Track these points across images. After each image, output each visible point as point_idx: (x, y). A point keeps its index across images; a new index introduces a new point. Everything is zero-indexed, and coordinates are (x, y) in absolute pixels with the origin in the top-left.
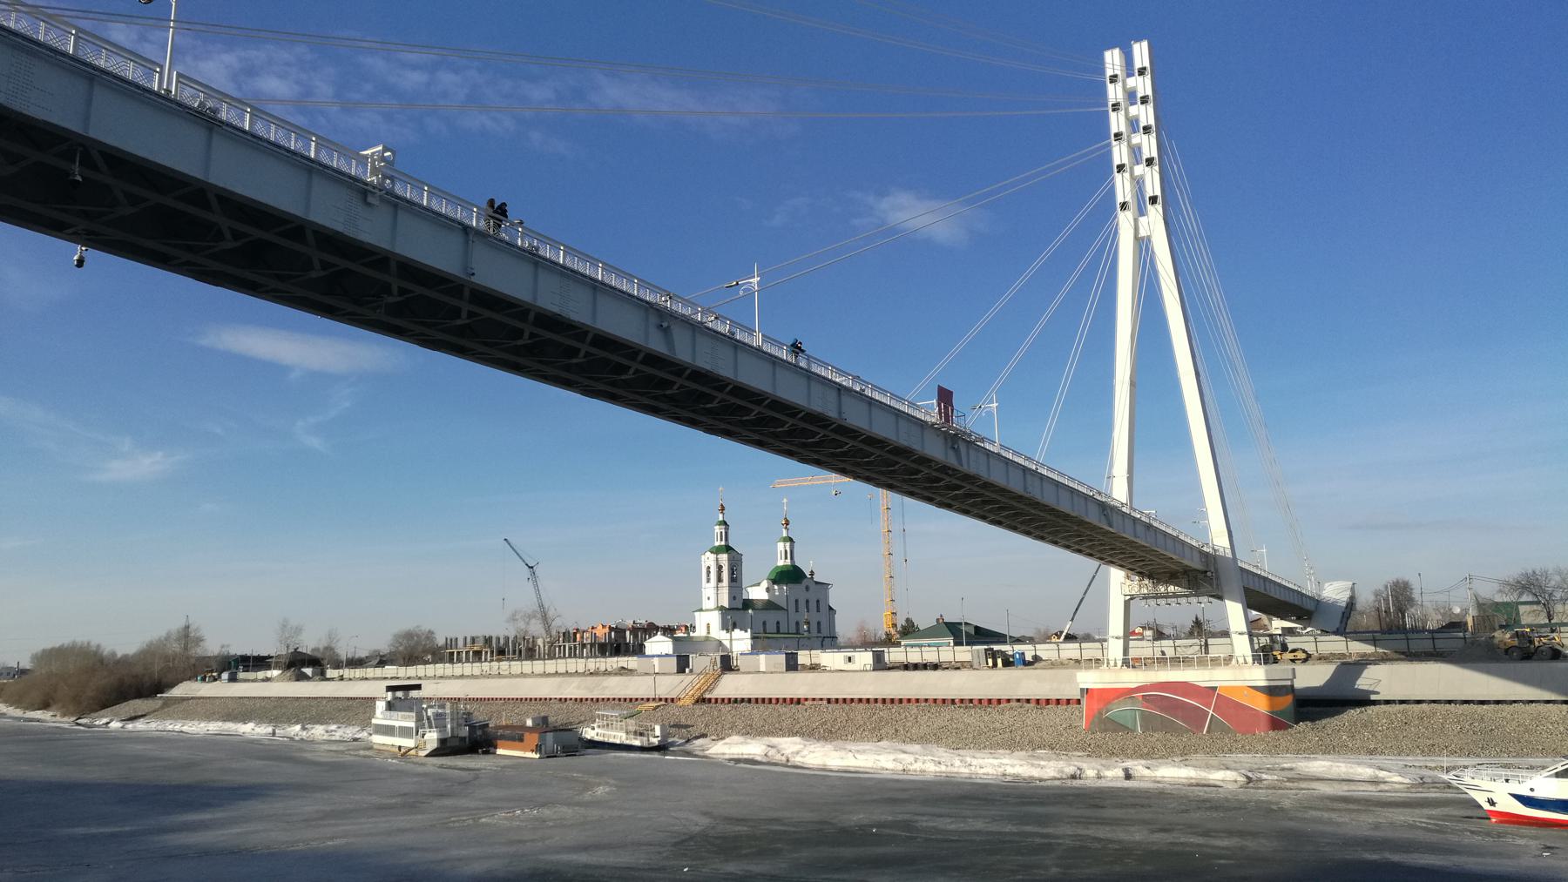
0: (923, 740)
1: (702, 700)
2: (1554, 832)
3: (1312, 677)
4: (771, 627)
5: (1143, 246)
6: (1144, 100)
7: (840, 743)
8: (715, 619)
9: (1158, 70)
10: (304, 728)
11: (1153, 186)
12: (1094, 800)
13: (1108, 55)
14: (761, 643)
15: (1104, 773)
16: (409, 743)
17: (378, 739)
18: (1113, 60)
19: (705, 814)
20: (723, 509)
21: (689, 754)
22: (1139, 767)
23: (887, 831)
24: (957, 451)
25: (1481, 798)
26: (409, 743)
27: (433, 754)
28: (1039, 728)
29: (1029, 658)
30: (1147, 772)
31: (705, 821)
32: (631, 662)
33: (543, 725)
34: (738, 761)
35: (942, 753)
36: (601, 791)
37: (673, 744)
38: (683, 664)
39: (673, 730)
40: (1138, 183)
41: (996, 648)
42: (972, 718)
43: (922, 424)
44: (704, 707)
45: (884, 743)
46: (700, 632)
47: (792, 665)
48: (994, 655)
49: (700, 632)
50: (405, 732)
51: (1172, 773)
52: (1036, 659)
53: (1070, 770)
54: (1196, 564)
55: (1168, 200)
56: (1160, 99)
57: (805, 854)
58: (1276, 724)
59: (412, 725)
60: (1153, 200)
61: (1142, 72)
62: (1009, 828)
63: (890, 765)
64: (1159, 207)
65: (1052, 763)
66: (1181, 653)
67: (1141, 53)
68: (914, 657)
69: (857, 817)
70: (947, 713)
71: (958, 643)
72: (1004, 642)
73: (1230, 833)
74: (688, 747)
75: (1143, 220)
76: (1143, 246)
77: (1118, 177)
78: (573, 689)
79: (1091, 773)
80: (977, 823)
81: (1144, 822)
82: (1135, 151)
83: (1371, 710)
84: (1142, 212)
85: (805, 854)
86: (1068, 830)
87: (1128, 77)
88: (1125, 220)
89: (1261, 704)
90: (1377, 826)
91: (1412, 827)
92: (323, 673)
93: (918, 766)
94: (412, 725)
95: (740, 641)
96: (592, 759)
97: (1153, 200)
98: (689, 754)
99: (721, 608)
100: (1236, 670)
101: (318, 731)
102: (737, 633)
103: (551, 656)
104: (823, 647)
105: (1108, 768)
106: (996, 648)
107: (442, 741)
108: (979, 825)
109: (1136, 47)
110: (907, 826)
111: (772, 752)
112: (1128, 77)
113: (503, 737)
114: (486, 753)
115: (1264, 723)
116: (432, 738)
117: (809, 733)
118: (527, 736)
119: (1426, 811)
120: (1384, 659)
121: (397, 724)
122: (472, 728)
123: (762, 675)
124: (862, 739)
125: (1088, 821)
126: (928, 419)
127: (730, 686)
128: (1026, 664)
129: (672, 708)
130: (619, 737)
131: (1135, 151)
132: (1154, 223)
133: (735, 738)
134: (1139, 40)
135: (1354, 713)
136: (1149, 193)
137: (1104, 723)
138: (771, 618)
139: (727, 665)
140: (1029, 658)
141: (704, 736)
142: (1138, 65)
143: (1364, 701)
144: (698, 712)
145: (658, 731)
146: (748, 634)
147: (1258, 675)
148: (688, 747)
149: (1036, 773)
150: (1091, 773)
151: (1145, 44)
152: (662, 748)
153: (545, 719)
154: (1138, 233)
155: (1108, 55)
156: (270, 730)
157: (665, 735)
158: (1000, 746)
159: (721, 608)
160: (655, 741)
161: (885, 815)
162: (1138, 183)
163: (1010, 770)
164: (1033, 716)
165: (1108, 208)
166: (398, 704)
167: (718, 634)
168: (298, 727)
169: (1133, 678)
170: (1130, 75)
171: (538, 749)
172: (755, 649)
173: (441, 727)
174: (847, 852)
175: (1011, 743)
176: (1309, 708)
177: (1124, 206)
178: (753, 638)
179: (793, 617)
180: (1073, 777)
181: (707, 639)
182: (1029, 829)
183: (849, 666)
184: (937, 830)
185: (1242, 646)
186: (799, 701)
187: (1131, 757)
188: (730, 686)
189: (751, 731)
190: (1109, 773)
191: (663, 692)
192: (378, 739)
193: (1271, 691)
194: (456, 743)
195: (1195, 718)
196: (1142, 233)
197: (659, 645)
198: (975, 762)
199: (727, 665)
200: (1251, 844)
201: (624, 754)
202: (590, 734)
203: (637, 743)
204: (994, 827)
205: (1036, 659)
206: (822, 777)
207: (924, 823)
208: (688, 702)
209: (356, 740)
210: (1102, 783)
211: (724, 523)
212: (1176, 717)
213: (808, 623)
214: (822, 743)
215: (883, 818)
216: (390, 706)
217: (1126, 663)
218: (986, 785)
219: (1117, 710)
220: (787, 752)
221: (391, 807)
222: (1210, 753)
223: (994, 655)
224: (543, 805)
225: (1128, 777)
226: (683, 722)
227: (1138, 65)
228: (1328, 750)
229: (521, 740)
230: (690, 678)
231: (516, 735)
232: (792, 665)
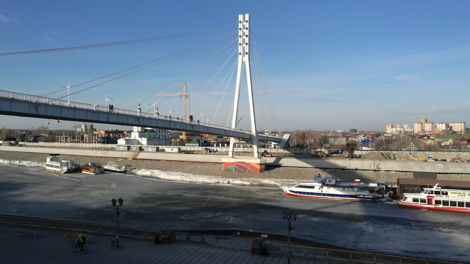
0: (187, 172)
1: (134, 159)
2: (292, 197)
3: (270, 160)
4: (152, 137)
5: (243, 63)
6: (247, 28)
7: (168, 172)
8: (137, 134)
9: (250, 22)
10: (20, 162)
11: (247, 50)
12: (217, 189)
13: (240, 15)
14: (150, 142)
15: (223, 182)
16: (59, 170)
17: (48, 168)
18: (241, 17)
19: (139, 192)
20: (140, 105)
21: (132, 173)
22: (231, 181)
23: (176, 197)
24: (193, 128)
25: (284, 190)
26: (59, 170)
27: (65, 173)
28: (213, 170)
29: (215, 150)
30: (232, 182)
31: (139, 194)
32: (114, 146)
33: (94, 165)
34: (144, 176)
35: (191, 176)
36: (114, 185)
37: (127, 171)
38: (129, 148)
39: (127, 167)
40: (244, 48)
41: (208, 148)
42: (199, 166)
43: (186, 124)
44: (135, 160)
45: (179, 173)
46: (133, 137)
47: (158, 150)
48: (207, 149)
49: (133, 137)
50: (57, 167)
51: (238, 182)
52: (217, 151)
53: (217, 181)
54: (248, 137)
55: (249, 53)
56: (250, 29)
57: (160, 202)
58: (261, 171)
59: (59, 165)
60: (247, 53)
61: (247, 21)
62: (200, 196)
63: (179, 179)
64: (248, 55)
65: (214, 179)
66: (249, 151)
67: (247, 16)
68: (188, 149)
69: (171, 193)
70: (194, 165)
71: (199, 146)
72: (210, 146)
73: (239, 197)
74: (131, 171)
75: (244, 57)
76: (243, 63)
77: (239, 56)
78: (99, 154)
79: (221, 182)
80: (194, 195)
81: (225, 195)
82: (244, 40)
83: (281, 168)
84: (244, 56)
85: (160, 202)
86: (210, 197)
87: (243, 20)
88: (240, 57)
89: (258, 167)
90: (265, 196)
91: (271, 196)
92: (17, 143)
93: (185, 179)
94: (59, 165)
95: (144, 141)
96: (108, 175)
97: (247, 53)
98: (132, 173)
99: (139, 132)
100: (255, 161)
101: (25, 163)
102: (143, 138)
103: (89, 142)
104: (166, 145)
105: (225, 180)
106: (208, 148)
107: (68, 170)
108: (194, 195)
109: (246, 15)
110: (180, 195)
111: (152, 174)
112: (243, 20)
113: (83, 168)
114: (80, 172)
115: (259, 171)
116: (65, 169)
117: (161, 169)
118: (91, 169)
119: (275, 192)
120: (290, 156)
121: (54, 165)
122: (76, 166)
123: (150, 153)
124: (174, 171)
125: (214, 195)
126: (186, 122)
127: (142, 155)
128: (214, 152)
129: (126, 161)
130: (114, 169)
131: (244, 40)
132: (246, 58)
133: (143, 170)
134: (247, 13)
135: (277, 169)
136: (246, 52)
137: (228, 170)
138: (152, 134)
139: (141, 149)
140: (215, 150)
141: (135, 169)
142: (246, 20)
143: (279, 166)
144: (133, 162)
145: (124, 167)
146: (146, 139)
147: (258, 161)
148: (131, 171)
149: (210, 181)
150: (221, 182)
151: (248, 15)
152: (125, 172)
153: (94, 163)
154: (243, 60)
155: (240, 15)
156: (9, 162)
157: (125, 168)
158: (204, 174)
159: (139, 132)
160: (123, 170)
161: (175, 193)
162: (244, 48)
163: (205, 181)
164: (213, 166)
165: (237, 54)
166: (53, 159)
167: (138, 138)
168: (18, 162)
169: (233, 160)
170: (244, 21)
171: (94, 172)
172: (148, 144)
173: (67, 166)
174: (168, 202)
175: (207, 173)
176: (268, 167)
177: (240, 54)
178: (147, 140)
179: (158, 134)
180: (217, 183)
181: (135, 139)
182: (203, 196)
183: (172, 151)
184: (186, 197)
185: (256, 155)
186: (159, 160)
187: (230, 178)
188: (142, 155)
189: (147, 168)
190: (225, 182)
191: (124, 156)
192: (48, 168)
193: (261, 164)
194: (72, 170)
195: (245, 169)
196: (244, 61)
197: (121, 142)
198: (198, 178)
199: (141, 149)
200: (241, 200)
201: (116, 174)
202: (106, 167)
203: (118, 170)
204: (197, 196)
205: (217, 151)
206: (164, 182)
207: (184, 195)
208: (131, 159)
209: (38, 166)
210: (223, 185)
211: (140, 109)
212: (241, 170)
213: (162, 136)
214: (164, 172)
215: (175, 194)
216: (51, 160)
217: (232, 157)
218: (199, 185)
219: (229, 167)
220: (156, 174)
221: (64, 190)
222: (246, 177)
223: (207, 149)
224: (102, 189)
225: (229, 183)
226: (130, 165)
227: (246, 20)
228: (269, 177)
229: (89, 170)
230: (131, 153)
231: (87, 168)
232: (158, 150)
